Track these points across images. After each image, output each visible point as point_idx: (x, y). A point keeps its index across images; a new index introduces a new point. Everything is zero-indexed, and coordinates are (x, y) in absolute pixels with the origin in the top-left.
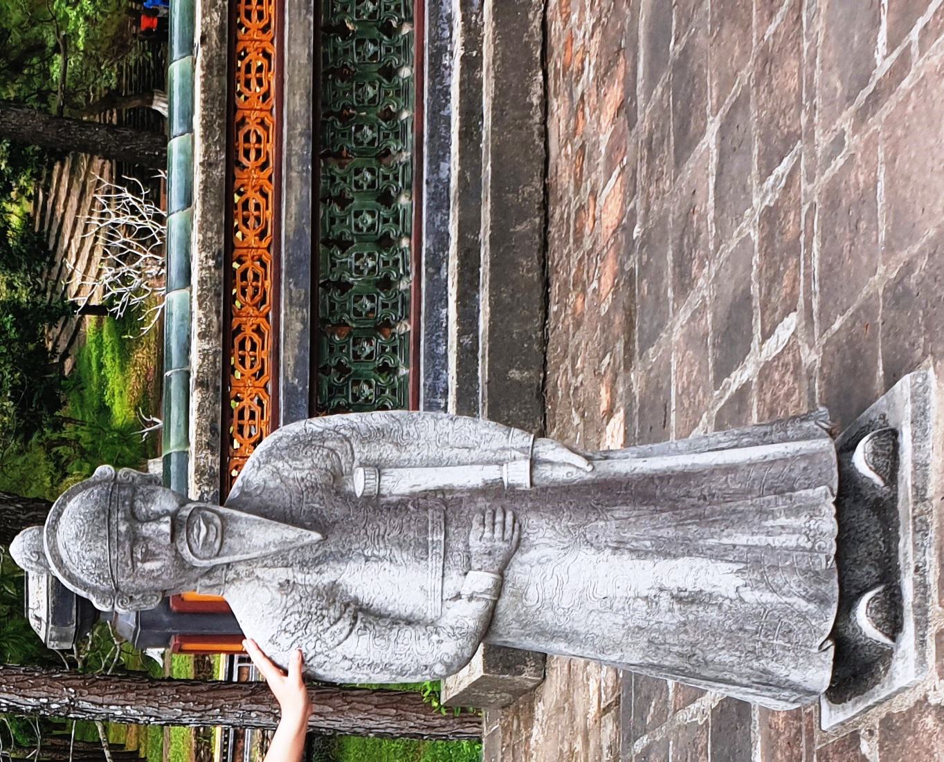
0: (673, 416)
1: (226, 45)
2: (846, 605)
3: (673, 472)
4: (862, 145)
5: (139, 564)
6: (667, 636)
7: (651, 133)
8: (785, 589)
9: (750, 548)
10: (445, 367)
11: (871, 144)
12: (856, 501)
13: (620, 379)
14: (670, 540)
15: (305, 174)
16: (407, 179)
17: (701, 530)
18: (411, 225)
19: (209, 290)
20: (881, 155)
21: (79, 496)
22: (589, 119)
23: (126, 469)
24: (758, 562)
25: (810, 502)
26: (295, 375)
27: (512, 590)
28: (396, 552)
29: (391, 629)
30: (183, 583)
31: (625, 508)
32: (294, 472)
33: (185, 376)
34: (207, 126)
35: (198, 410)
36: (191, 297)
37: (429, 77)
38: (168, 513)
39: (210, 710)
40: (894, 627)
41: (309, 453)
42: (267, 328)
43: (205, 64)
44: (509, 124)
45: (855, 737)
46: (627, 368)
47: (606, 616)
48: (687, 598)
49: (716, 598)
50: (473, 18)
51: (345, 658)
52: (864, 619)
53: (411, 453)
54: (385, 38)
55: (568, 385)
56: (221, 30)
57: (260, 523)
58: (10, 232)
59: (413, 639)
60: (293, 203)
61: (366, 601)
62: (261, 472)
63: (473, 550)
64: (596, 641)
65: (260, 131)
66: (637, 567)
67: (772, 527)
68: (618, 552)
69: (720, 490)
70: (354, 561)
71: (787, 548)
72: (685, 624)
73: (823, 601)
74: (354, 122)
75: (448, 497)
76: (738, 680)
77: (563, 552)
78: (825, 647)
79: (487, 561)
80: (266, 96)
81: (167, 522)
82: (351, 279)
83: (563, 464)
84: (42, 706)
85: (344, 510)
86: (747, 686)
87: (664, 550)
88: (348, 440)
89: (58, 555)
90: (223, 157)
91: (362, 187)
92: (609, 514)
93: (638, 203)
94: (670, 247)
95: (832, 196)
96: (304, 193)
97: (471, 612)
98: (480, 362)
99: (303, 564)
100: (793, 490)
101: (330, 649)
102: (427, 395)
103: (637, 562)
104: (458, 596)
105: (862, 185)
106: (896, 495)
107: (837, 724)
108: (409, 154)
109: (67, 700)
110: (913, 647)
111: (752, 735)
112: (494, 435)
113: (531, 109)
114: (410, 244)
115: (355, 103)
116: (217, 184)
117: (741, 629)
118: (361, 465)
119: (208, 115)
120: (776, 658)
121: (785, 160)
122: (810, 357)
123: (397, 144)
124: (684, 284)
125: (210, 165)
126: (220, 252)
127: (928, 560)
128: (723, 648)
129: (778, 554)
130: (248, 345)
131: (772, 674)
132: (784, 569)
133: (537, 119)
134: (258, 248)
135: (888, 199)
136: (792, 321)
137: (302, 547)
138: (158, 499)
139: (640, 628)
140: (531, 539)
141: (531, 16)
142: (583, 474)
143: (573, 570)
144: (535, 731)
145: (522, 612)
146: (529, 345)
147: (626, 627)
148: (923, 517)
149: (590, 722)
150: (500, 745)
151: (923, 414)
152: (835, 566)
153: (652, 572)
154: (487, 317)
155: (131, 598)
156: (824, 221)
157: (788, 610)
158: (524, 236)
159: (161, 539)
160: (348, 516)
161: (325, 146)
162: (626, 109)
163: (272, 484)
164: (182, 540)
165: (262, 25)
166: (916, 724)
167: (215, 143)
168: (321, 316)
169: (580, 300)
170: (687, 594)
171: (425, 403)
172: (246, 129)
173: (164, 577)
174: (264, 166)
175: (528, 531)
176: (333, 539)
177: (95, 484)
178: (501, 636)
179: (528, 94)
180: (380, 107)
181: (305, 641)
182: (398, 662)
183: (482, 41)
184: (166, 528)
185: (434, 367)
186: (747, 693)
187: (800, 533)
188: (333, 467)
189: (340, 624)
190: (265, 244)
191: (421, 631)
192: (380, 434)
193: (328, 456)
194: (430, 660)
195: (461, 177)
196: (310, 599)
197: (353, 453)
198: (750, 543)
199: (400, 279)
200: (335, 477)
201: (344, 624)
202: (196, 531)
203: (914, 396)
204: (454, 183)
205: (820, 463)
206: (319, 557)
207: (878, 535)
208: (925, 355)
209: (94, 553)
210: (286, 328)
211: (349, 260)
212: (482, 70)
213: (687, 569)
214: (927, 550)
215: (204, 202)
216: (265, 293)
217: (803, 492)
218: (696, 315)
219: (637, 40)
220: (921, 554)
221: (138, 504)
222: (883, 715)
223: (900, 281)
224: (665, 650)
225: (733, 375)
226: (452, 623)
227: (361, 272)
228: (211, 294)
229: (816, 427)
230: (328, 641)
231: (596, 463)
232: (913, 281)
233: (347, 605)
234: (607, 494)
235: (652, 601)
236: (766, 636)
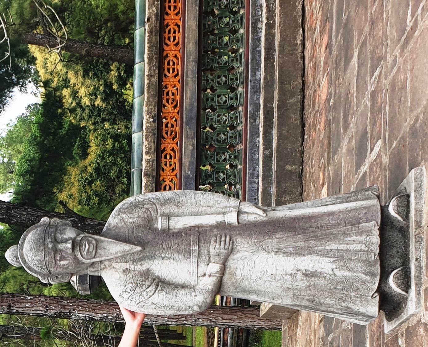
1: (159, 22)
5: (58, 262)
6: (302, 292)
7: (337, 57)
8: (355, 270)
10: (258, 164)
11: (406, 62)
12: (392, 228)
13: (326, 169)
15: (194, 79)
16: (242, 80)
17: (316, 243)
19: (150, 132)
20: (409, 67)
21: (31, 233)
22: (318, 51)
24: (342, 257)
26: (189, 170)
27: (229, 272)
28: (176, 255)
29: (174, 290)
31: (281, 233)
32: (130, 219)
33: (140, 171)
34: (150, 59)
35: (145, 186)
36: (143, 136)
38: (71, 239)
39: (180, 318)
40: (407, 287)
41: (137, 211)
42: (177, 149)
43: (149, 30)
44: (287, 53)
47: (273, 283)
48: (309, 274)
49: (323, 274)
50: (271, 6)
51: (153, 303)
52: (392, 283)
53: (184, 209)
54: (232, 16)
55: (310, 172)
56: (157, 15)
57: (114, 243)
58: (126, 103)
60: (189, 92)
61: (163, 277)
62: (115, 219)
63: (211, 254)
65: (175, 60)
66: (287, 260)
68: (278, 254)
69: (326, 224)
70: (157, 260)
71: (356, 251)
72: (309, 286)
73: (373, 275)
76: (337, 312)
77: (252, 254)
78: (374, 296)
79: (217, 258)
80: (177, 44)
81: (70, 243)
82: (216, 126)
84: (104, 317)
85: (153, 236)
86: (342, 314)
87: (299, 252)
88: (155, 204)
90: (157, 72)
91: (221, 84)
92: (273, 236)
93: (332, 88)
95: (393, 84)
98: (273, 162)
99: (134, 261)
100: (359, 223)
101: (146, 299)
102: (249, 177)
103: (286, 258)
104: (205, 275)
105: (402, 81)
106: (409, 225)
107: (390, 331)
108: (243, 68)
109: (115, 315)
111: (366, 334)
112: (222, 201)
113: (297, 46)
114: (243, 109)
116: (154, 84)
117: (335, 288)
118: (161, 215)
119: (150, 54)
120: (352, 301)
121: (378, 69)
122: (385, 160)
123: (237, 64)
125: (151, 76)
126: (155, 115)
127: (422, 255)
128: (328, 297)
129: (352, 253)
130: (168, 157)
131: (352, 309)
132: (354, 260)
133: (300, 51)
134: (173, 113)
136: (380, 143)
137: (133, 253)
138: (67, 233)
141: (297, 4)
142: (262, 218)
143: (257, 262)
144: (298, 330)
147: (282, 288)
149: (316, 326)
151: (420, 187)
152: (378, 258)
153: (293, 262)
154: (276, 142)
155: (57, 277)
157: (357, 279)
158: (293, 105)
160: (154, 239)
161: (204, 66)
162: (329, 46)
163: (120, 225)
165: (176, 12)
166: (417, 332)
167: (153, 66)
168: (202, 143)
169: (314, 133)
170: (310, 272)
172: (168, 59)
173: (70, 267)
174: (177, 75)
175: (237, 245)
177: (40, 226)
178: (226, 292)
180: (229, 48)
182: (177, 305)
183: (275, 16)
184: (69, 246)
185: (253, 164)
186: (344, 317)
187: (362, 243)
189: (150, 288)
190: (176, 111)
191: (187, 291)
192: (169, 201)
193: (145, 212)
194: (191, 304)
195: (265, 78)
196: (137, 277)
197: (157, 210)
198: (339, 248)
199: (238, 125)
200: (149, 221)
201: (152, 288)
202: (83, 247)
203: (416, 179)
205: (373, 210)
206: (141, 258)
207: (402, 244)
208: (422, 160)
209: (38, 257)
211: (215, 117)
212: (275, 29)
213: (309, 261)
214: (422, 251)
215: (148, 93)
216: (176, 133)
217: (364, 224)
218: (351, 139)
220: (418, 252)
221: (58, 235)
222: (406, 327)
223: (414, 125)
224: (301, 298)
225: (361, 168)
226: (202, 287)
227: (221, 123)
229: (371, 194)
230: (145, 296)
231: (268, 213)
232: (418, 125)
233: (154, 279)
236: (347, 291)
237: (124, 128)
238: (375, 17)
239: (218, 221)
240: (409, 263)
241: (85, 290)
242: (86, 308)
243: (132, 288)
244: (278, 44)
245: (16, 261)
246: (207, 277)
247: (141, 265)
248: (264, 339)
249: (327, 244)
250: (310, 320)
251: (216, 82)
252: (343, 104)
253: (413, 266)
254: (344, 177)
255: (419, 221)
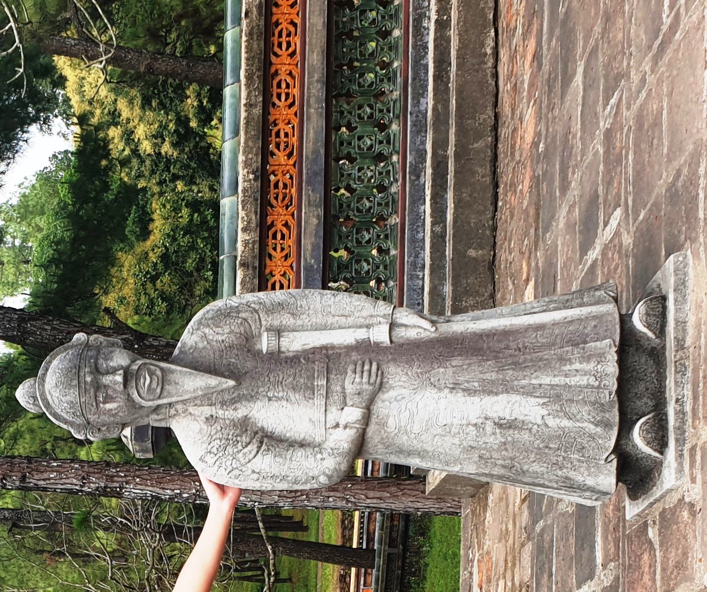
0: (559, 284)
2: (625, 427)
3: (496, 330)
4: (655, 82)
5: (101, 405)
8: (578, 417)
9: (552, 386)
10: (423, 248)
11: (660, 81)
12: (637, 350)
13: (533, 256)
14: (493, 382)
15: (320, 110)
16: (397, 112)
17: (516, 374)
18: (398, 145)
19: (250, 197)
20: (665, 90)
22: (519, 65)
23: (96, 336)
24: (558, 397)
25: (598, 352)
26: (312, 257)
28: (291, 394)
29: (287, 450)
30: (136, 419)
31: (460, 358)
32: (217, 336)
34: (249, 77)
36: (238, 202)
37: (413, 36)
38: (122, 368)
40: (661, 445)
42: (292, 223)
43: (248, 32)
44: (469, 69)
45: (646, 525)
46: (536, 250)
47: (447, 438)
48: (506, 424)
49: (527, 424)
51: (253, 472)
52: (638, 438)
53: (304, 320)
57: (191, 374)
59: (303, 457)
60: (312, 131)
61: (270, 430)
62: (194, 336)
63: (347, 391)
64: (441, 457)
66: (469, 402)
67: (569, 370)
69: (531, 343)
71: (580, 386)
72: (505, 444)
73: (607, 425)
74: (358, 70)
75: (330, 352)
76: (550, 485)
78: (609, 459)
79: (357, 399)
81: (120, 374)
82: (355, 186)
83: (415, 326)
84: (176, 496)
85: (254, 363)
86: (557, 489)
87: (489, 389)
88: (256, 312)
89: (47, 399)
90: (261, 99)
91: (363, 118)
94: (558, 158)
95: (640, 118)
96: (320, 124)
97: (346, 437)
98: (447, 245)
99: (223, 403)
100: (585, 342)
101: (242, 465)
103: (468, 398)
104: (337, 426)
105: (655, 112)
106: (665, 345)
108: (398, 93)
109: (194, 491)
110: (674, 459)
113: (485, 57)
114: (399, 159)
115: (359, 57)
117: (547, 447)
118: (268, 330)
119: (249, 69)
121: (616, 93)
122: (627, 240)
123: (389, 86)
124: (565, 188)
126: (257, 168)
128: (534, 461)
130: (279, 236)
131: (573, 480)
134: (287, 165)
135: (668, 122)
136: (618, 212)
137: (222, 391)
138: (115, 358)
139: (472, 448)
140: (390, 382)
142: (429, 333)
144: (488, 515)
145: (384, 436)
146: (483, 231)
147: (462, 446)
148: (682, 361)
149: (517, 509)
150: (470, 524)
152: (616, 398)
153: (479, 405)
154: (452, 212)
155: (99, 429)
156: (635, 139)
157: (581, 432)
158: (478, 152)
159: (117, 387)
160: (256, 368)
161: (336, 89)
162: (537, 57)
163: (200, 345)
164: (132, 387)
166: (678, 517)
167: (255, 90)
170: (506, 421)
171: (408, 275)
175: (389, 377)
176: (244, 385)
177: (72, 347)
178: (371, 454)
179: (484, 46)
180: (377, 59)
181: (224, 460)
182: (292, 475)
183: (451, 8)
184: (119, 378)
185: (415, 248)
187: (590, 375)
188: (245, 332)
189: (249, 447)
190: (291, 162)
191: (309, 451)
193: (241, 323)
195: (435, 109)
197: (260, 321)
199: (391, 184)
200: (247, 339)
201: (253, 447)
202: (142, 380)
203: (676, 270)
204: (430, 113)
206: (234, 398)
207: (653, 375)
208: (686, 240)
210: (306, 222)
212: (450, 29)
213: (505, 402)
214: (685, 386)
215: (246, 133)
217: (593, 344)
219: (543, 5)
220: (680, 389)
221: (101, 361)
222: (661, 510)
223: (673, 184)
224: (492, 463)
225: (588, 254)
226: (332, 445)
227: (363, 181)
228: (251, 200)
229: (605, 295)
230: (241, 459)
231: (438, 325)
232: (680, 184)
233: (256, 433)
234: (447, 348)
235: (480, 427)
236: (565, 452)
237: (207, 190)
238: (612, 10)
239: (358, 338)
240: (666, 407)
241: (144, 451)
242: (147, 480)
243: (220, 446)
244: (455, 53)
245: (33, 404)
246: (340, 429)
247: (235, 409)
248: (432, 531)
249: (533, 376)
250: (507, 499)
251: (355, 115)
252: (559, 150)
253: (671, 410)
254: (562, 269)
255: (681, 338)
